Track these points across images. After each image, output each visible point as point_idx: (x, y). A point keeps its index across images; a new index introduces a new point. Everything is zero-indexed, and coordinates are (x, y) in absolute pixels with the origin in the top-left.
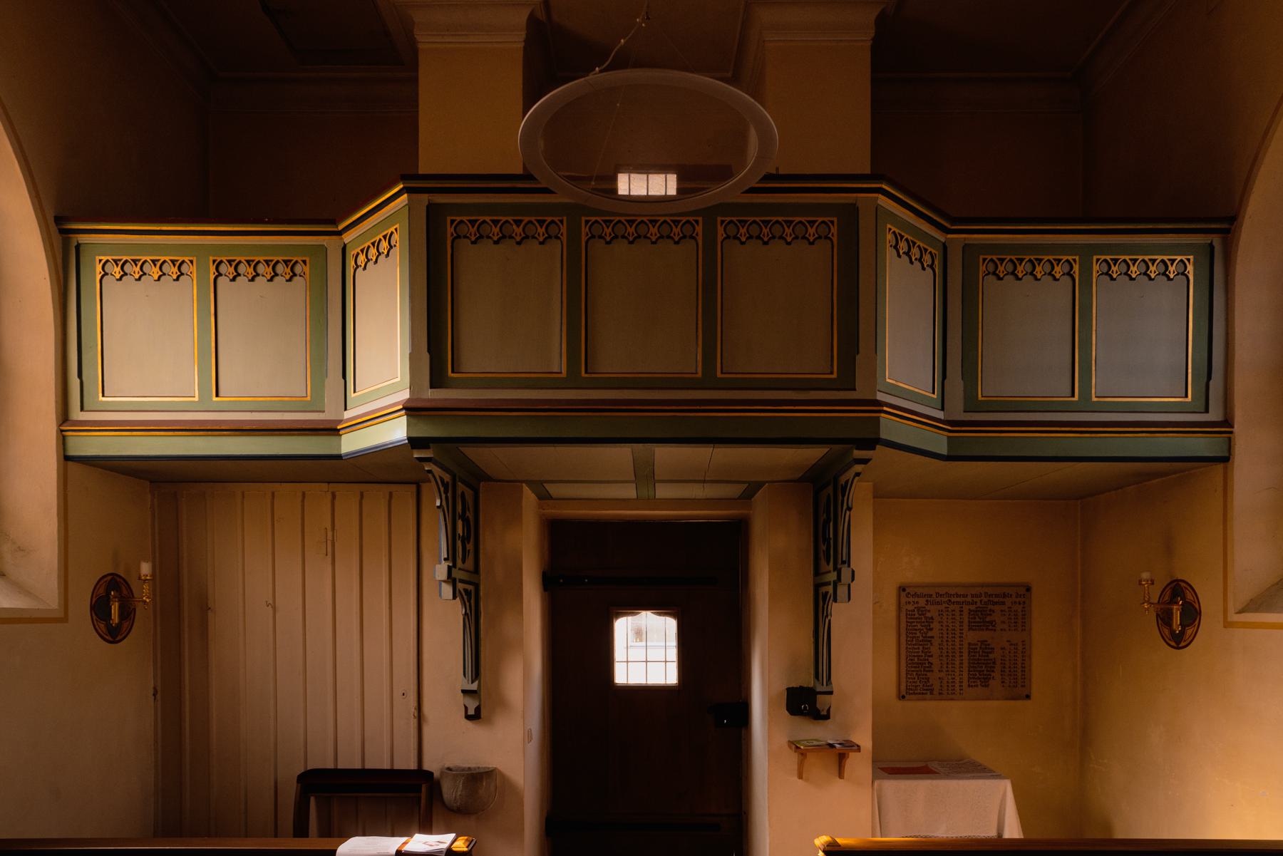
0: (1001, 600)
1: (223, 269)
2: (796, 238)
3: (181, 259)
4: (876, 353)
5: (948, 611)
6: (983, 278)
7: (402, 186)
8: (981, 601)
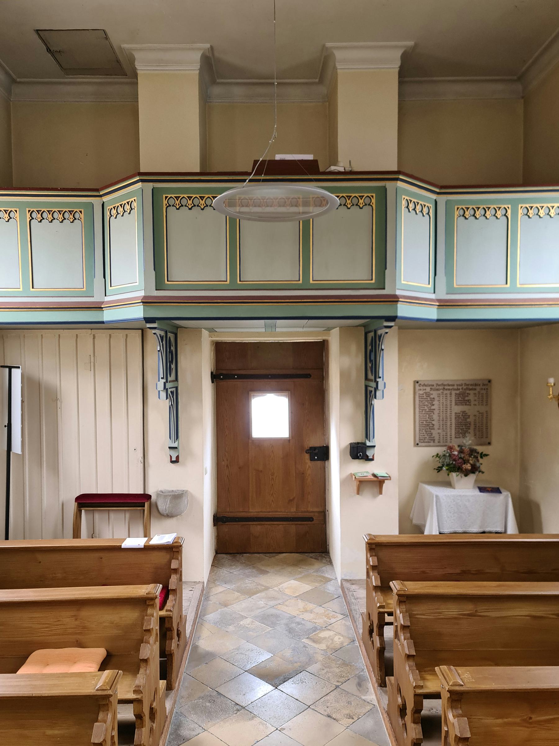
0: (474, 387)
1: (34, 215)
2: (353, 205)
3: (10, 209)
4: (396, 269)
5: (443, 394)
6: (457, 218)
7: (138, 178)
8: (462, 388)
